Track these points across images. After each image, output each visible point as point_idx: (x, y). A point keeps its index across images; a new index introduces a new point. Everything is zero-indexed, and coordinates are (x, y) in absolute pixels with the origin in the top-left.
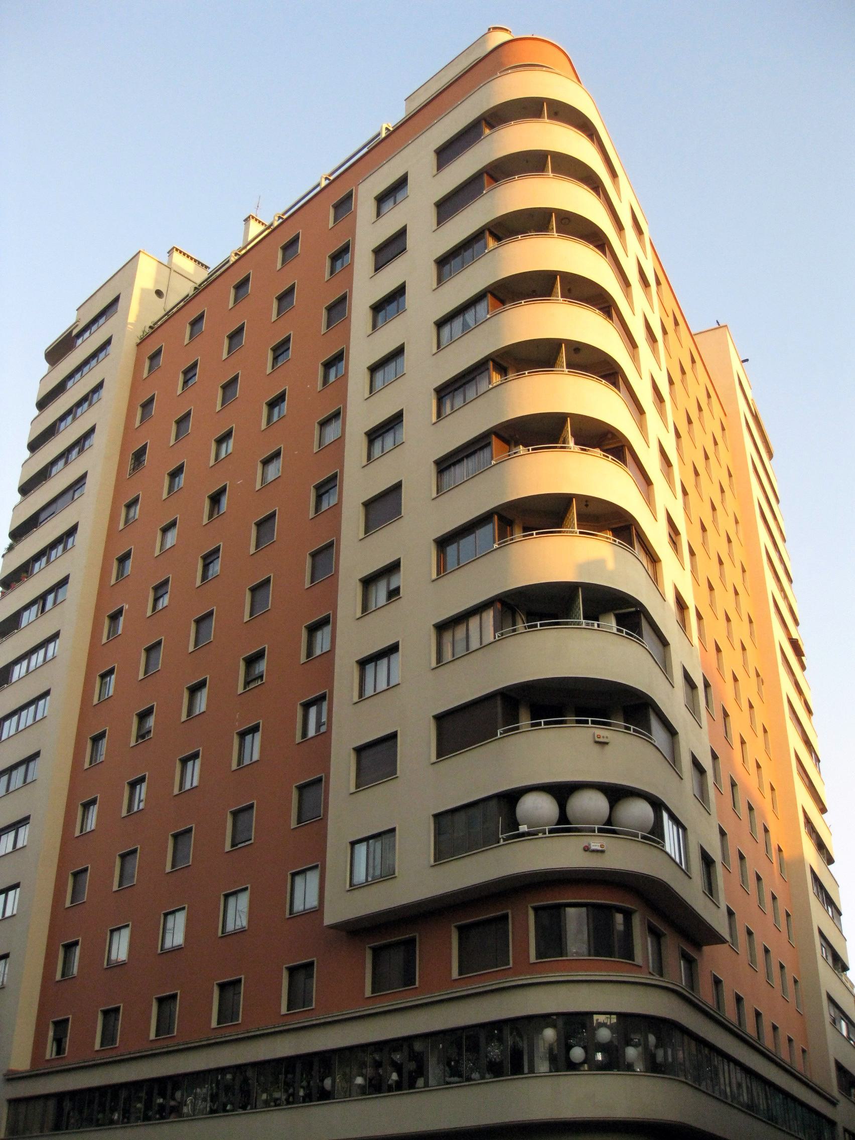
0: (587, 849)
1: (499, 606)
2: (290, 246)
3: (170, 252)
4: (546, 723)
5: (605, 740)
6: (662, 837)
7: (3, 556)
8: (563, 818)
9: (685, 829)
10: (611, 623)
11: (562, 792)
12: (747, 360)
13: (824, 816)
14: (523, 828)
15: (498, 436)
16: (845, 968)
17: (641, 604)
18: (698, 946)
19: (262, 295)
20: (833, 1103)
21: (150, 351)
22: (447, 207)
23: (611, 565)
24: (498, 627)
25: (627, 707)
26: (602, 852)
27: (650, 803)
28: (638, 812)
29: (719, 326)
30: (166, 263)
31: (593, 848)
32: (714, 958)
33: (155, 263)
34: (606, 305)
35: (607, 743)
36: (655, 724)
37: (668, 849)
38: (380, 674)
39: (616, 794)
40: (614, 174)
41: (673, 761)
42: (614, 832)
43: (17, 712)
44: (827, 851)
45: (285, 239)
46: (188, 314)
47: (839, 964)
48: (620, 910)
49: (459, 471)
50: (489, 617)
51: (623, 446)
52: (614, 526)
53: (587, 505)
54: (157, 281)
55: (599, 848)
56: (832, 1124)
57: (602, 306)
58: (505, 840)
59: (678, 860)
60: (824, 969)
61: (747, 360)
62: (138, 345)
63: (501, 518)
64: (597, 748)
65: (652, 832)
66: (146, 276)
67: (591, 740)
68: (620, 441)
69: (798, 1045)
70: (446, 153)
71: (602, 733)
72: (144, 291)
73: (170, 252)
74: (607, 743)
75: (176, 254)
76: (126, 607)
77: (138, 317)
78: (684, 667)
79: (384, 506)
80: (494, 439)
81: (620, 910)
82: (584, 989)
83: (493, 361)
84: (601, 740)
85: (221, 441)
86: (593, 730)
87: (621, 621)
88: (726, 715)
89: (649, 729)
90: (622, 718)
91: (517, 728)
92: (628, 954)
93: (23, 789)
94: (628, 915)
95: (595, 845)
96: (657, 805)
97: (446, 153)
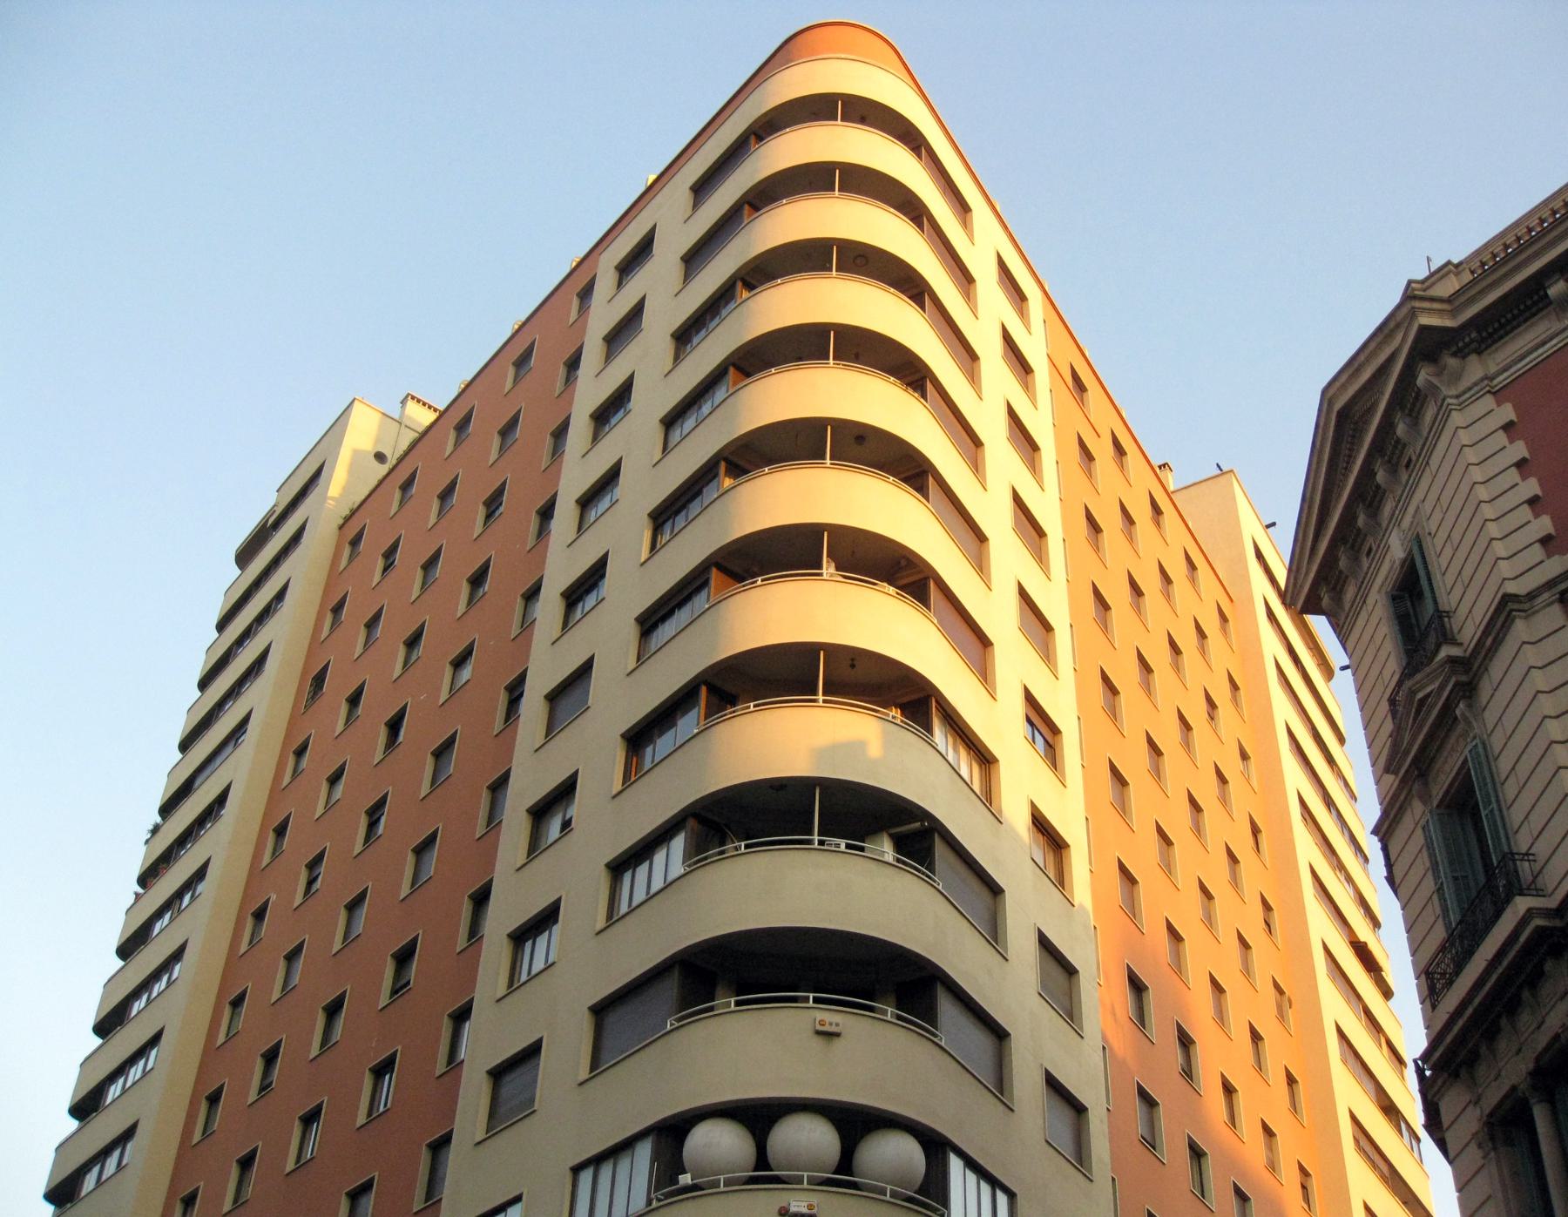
1: (691, 823)
2: (522, 362)
3: (403, 402)
4: (816, 1000)
6: (944, 1200)
7: (147, 842)
8: (762, 1161)
9: (1011, 1195)
10: (885, 848)
11: (758, 1117)
12: (1274, 524)
14: (685, 1179)
15: (722, 569)
17: (926, 815)
21: (352, 535)
22: (694, 258)
23: (875, 750)
24: (687, 856)
25: (902, 984)
27: (922, 1143)
28: (894, 1153)
29: (1222, 472)
30: (397, 417)
33: (376, 417)
34: (917, 377)
35: (838, 1035)
36: (939, 734)
38: (541, 950)
39: (854, 1123)
40: (962, 207)
41: (1000, 1084)
42: (854, 1186)
45: (519, 355)
46: (401, 476)
49: (667, 630)
50: (678, 843)
51: (926, 579)
52: (905, 700)
53: (853, 666)
54: (378, 441)
57: (910, 379)
58: (659, 1200)
61: (1274, 524)
62: (341, 527)
63: (712, 689)
64: (818, 1043)
65: (922, 1190)
66: (363, 434)
67: (810, 1033)
68: (920, 572)
70: (702, 189)
71: (831, 1018)
72: (357, 453)
73: (403, 402)
74: (838, 1035)
75: (410, 404)
76: (274, 897)
77: (346, 489)
79: (571, 689)
80: (714, 574)
83: (726, 460)
84: (826, 1028)
85: (459, 663)
86: (820, 1015)
87: (901, 845)
88: (1185, 1041)
90: (892, 999)
91: (711, 1009)
93: (119, 1176)
96: (936, 1146)
97: (702, 189)
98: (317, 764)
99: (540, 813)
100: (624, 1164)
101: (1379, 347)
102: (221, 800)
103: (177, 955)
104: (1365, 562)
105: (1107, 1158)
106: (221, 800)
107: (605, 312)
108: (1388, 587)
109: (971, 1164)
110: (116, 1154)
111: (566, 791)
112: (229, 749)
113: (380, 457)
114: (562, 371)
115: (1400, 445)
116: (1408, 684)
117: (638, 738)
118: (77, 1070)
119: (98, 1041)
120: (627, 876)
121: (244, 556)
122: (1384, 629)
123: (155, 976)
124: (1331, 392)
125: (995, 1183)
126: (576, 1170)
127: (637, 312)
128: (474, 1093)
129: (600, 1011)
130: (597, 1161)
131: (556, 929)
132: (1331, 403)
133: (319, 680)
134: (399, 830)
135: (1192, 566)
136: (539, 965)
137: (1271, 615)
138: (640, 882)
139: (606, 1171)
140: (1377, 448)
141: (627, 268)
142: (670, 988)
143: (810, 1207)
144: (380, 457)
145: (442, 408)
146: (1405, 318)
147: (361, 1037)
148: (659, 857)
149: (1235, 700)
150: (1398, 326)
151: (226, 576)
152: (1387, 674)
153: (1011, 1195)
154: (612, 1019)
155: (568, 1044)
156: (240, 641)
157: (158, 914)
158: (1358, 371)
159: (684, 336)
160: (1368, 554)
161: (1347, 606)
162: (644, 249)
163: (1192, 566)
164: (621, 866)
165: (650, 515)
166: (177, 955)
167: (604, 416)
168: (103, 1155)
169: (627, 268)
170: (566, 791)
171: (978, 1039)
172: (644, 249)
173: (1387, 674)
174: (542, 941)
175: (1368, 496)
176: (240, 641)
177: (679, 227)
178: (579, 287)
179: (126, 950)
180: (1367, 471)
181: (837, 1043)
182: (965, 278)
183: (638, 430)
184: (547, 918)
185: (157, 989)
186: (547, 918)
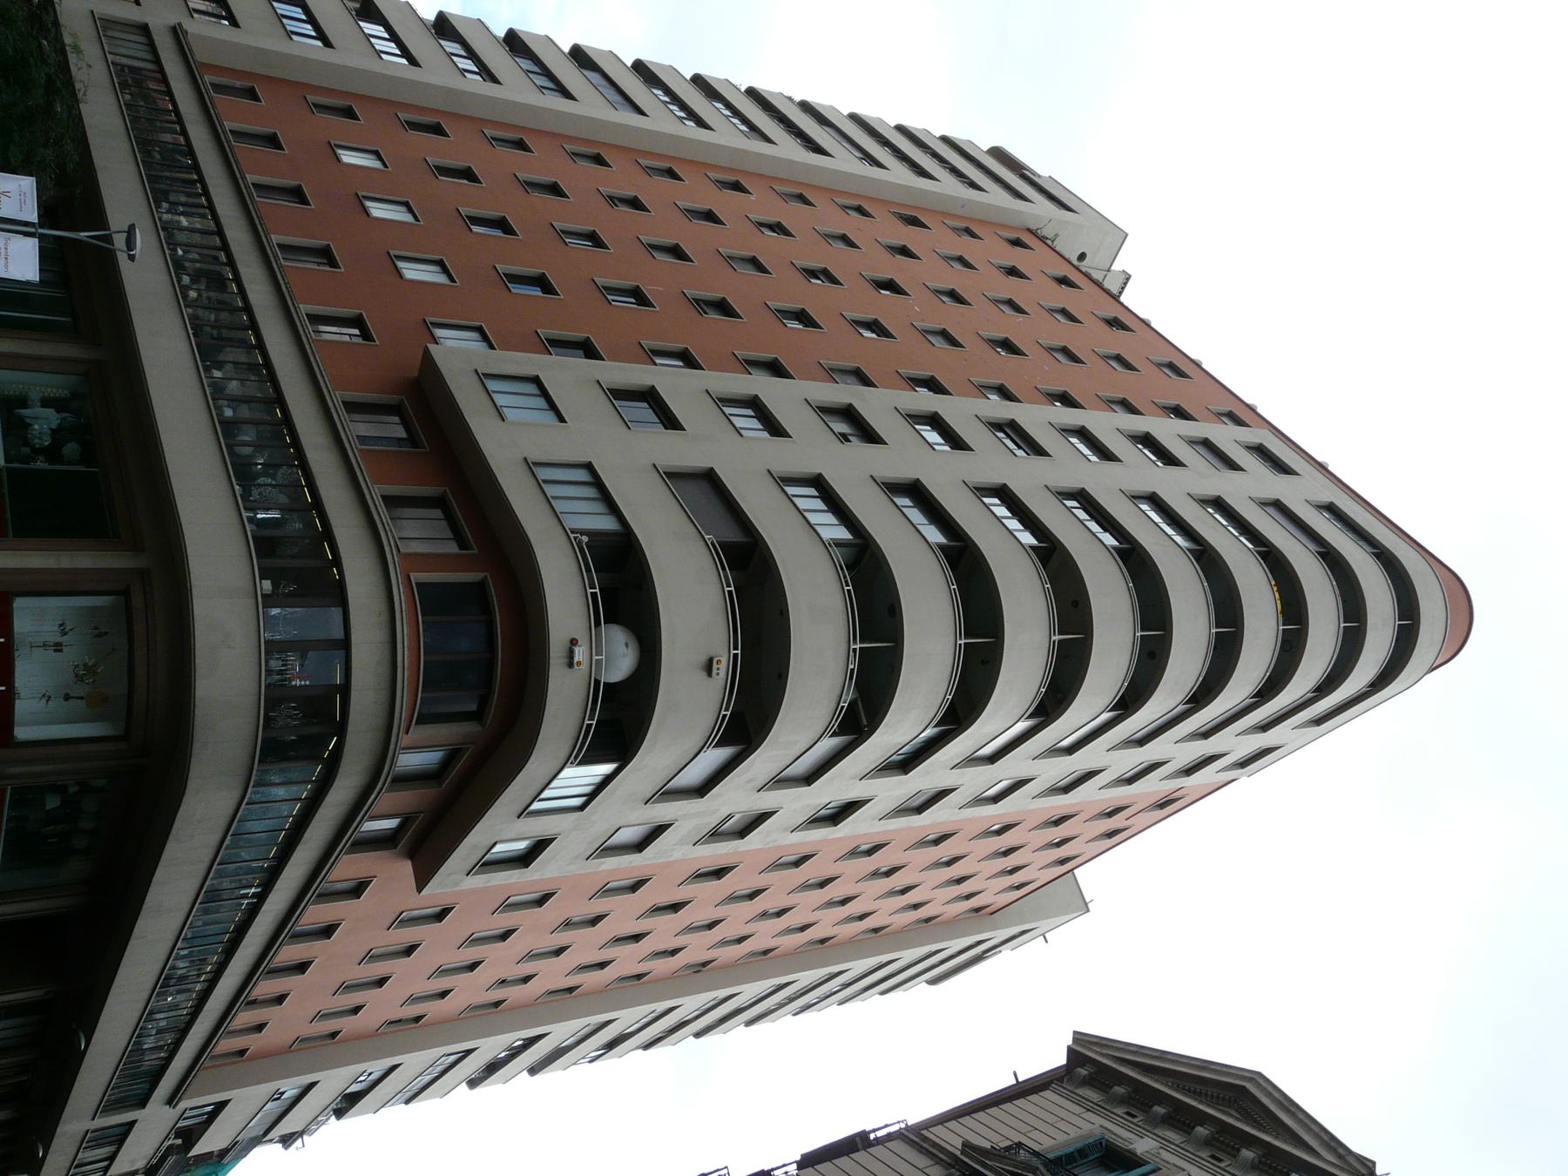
0: (574, 642)
5: (714, 671)
9: (582, 808)
13: (525, 1073)
16: (339, 1113)
17: (873, 728)
18: (412, 854)
19: (1115, 342)
20: (171, 1100)
26: (571, 665)
31: (577, 650)
32: (395, 872)
36: (723, 753)
37: (568, 772)
38: (747, 422)
43: (471, 54)
44: (485, 1078)
45: (1178, 366)
47: (347, 1103)
48: (484, 702)
50: (843, 534)
55: (576, 660)
56: (142, 1103)
59: (546, 794)
60: (333, 1082)
64: (703, 658)
67: (712, 654)
69: (253, 1042)
70: (1331, 509)
78: (773, 813)
81: (484, 702)
82: (380, 636)
84: (715, 666)
86: (724, 660)
89: (720, 744)
92: (424, 719)
94: (477, 716)
95: (580, 654)
97: (1331, 509)
98: (851, 224)
99: (848, 413)
100: (599, 507)
101: (1317, 1136)
102: (819, 150)
103: (701, 123)
104: (1120, 1111)
105: (604, 867)
106: (819, 150)
107: (1226, 436)
108: (1108, 1136)
109: (608, 779)
110: (551, 85)
111: (870, 435)
112: (858, 154)
113: (1082, 257)
114: (1173, 402)
115: (1234, 1153)
116: (1035, 1161)
117: (917, 492)
118: (606, 48)
119: (566, 49)
120: (812, 491)
121: (998, 153)
122: (1073, 1133)
123: (683, 106)
124: (1351, 1160)
125: (591, 796)
126: (589, 467)
127: (1232, 466)
128: (638, 375)
129: (710, 478)
130: (598, 483)
131: (765, 434)
132: (1250, 1080)
133: (914, 222)
134: (813, 296)
135: (1019, 887)
136: (739, 422)
137: (979, 943)
138: (809, 501)
139: (590, 492)
140: (1224, 1128)
141: (1261, 451)
142: (733, 535)
143: (579, 663)
144: (1082, 257)
145: (1122, 299)
146: (1350, 1165)
147: (658, 277)
148: (830, 518)
149: (919, 921)
150: (1340, 1157)
151: (982, 140)
152: (1035, 1135)
153: (582, 808)
154: (701, 491)
155: (684, 452)
156: (935, 155)
157: (729, 106)
158: (1287, 1111)
159: (1219, 504)
160: (1128, 1113)
161: (1080, 1091)
162: (1281, 468)
163: (1019, 887)
164: (819, 484)
165: (936, 413)
166: (701, 123)
167: (1147, 441)
168: (471, 54)
169: (1261, 451)
170: (870, 435)
171: (695, 773)
172: (1281, 468)
173: (1035, 1135)
174: (755, 424)
175: (1181, 1119)
176: (935, 155)
177: (1298, 494)
178: (1239, 414)
179: (639, 67)
180: (1204, 1119)
181: (704, 674)
182: (1265, 727)
183: (1143, 471)
184: (774, 428)
185: (735, 121)
186: (774, 428)
